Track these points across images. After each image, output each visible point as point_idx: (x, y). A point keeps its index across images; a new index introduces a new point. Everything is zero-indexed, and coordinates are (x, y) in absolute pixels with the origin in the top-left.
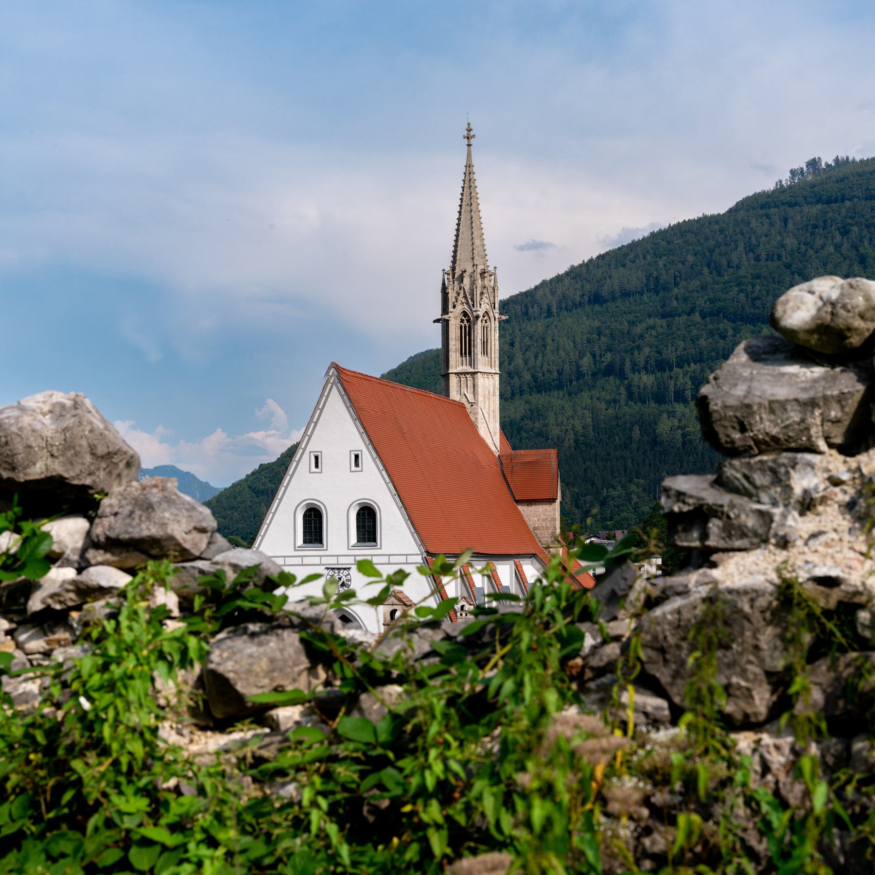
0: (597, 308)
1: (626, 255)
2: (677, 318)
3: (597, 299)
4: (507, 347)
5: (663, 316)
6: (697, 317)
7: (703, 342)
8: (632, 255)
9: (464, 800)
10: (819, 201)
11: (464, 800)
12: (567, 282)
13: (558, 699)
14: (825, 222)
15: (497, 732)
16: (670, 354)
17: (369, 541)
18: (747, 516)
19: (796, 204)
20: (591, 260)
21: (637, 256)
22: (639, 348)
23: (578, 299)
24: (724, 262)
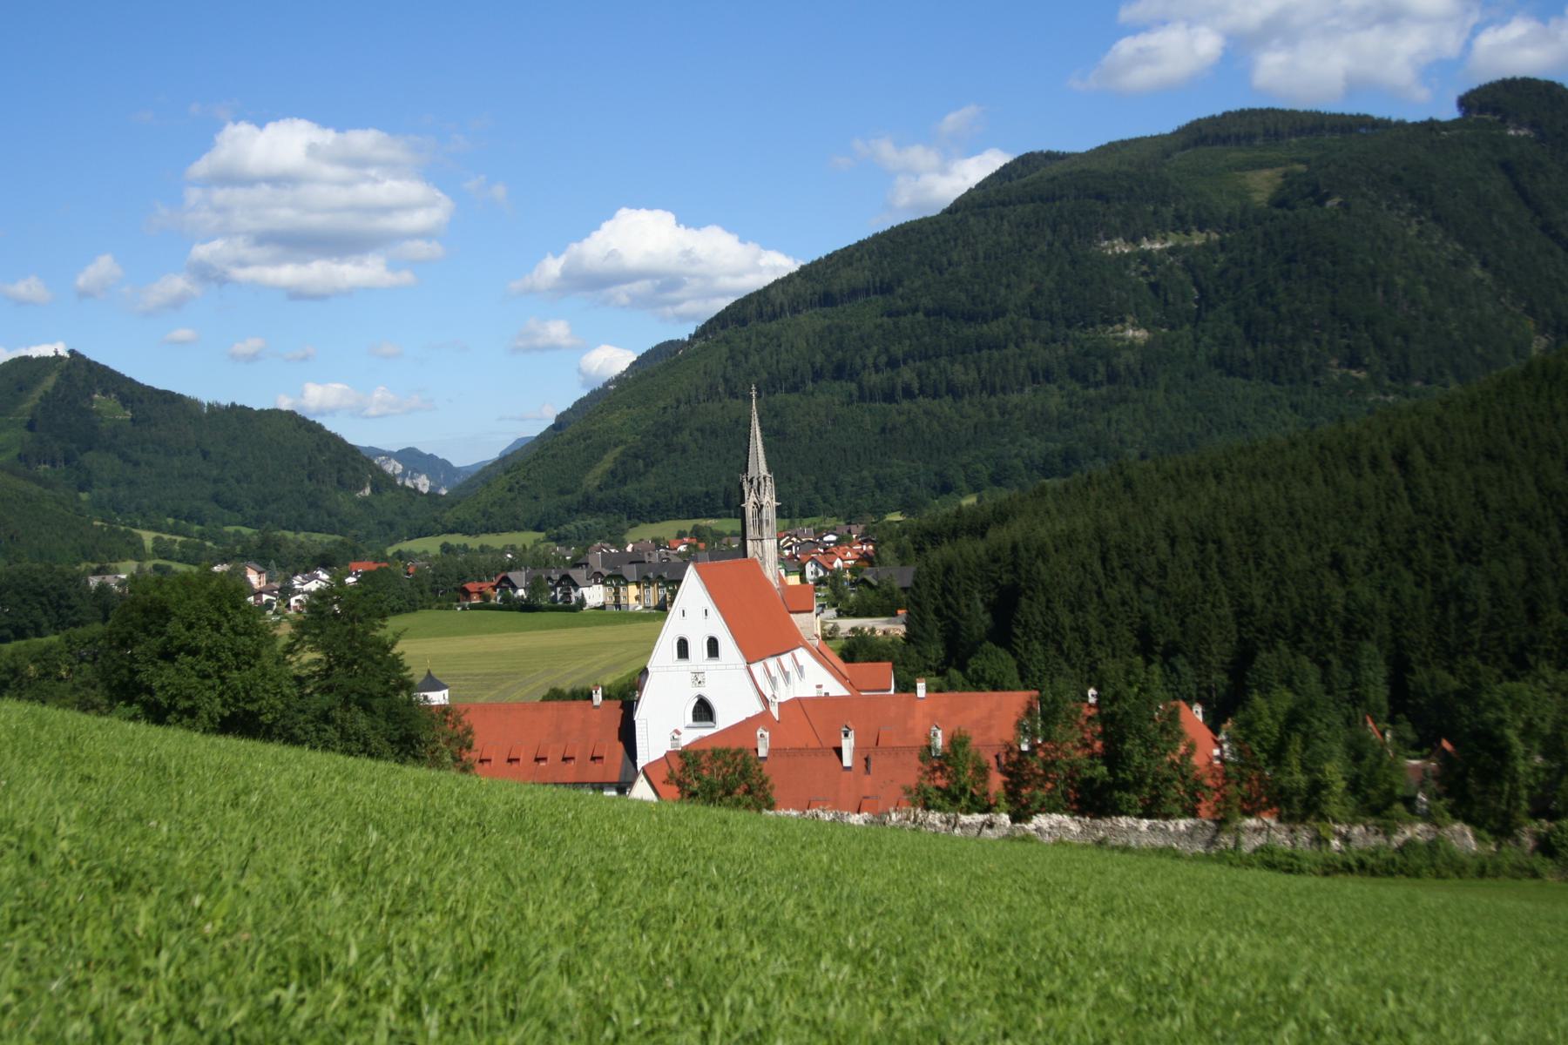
0: (827, 310)
1: (851, 256)
2: (903, 318)
3: (827, 300)
4: (752, 309)
5: (890, 315)
6: (920, 316)
7: (927, 339)
8: (858, 255)
9: (1206, 939)
10: (1033, 201)
11: (1206, 939)
12: (798, 280)
13: (624, 760)
14: (1037, 222)
15: (1413, 313)
16: (898, 351)
17: (706, 720)
18: (367, 991)
19: (1010, 203)
20: (820, 260)
21: (862, 256)
22: (868, 347)
23: (809, 298)
24: (945, 260)
